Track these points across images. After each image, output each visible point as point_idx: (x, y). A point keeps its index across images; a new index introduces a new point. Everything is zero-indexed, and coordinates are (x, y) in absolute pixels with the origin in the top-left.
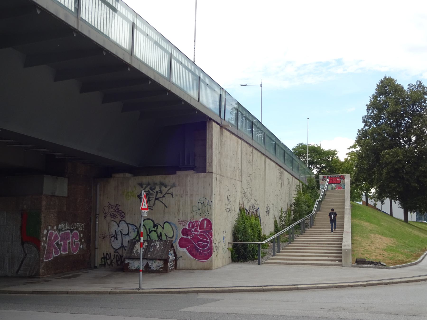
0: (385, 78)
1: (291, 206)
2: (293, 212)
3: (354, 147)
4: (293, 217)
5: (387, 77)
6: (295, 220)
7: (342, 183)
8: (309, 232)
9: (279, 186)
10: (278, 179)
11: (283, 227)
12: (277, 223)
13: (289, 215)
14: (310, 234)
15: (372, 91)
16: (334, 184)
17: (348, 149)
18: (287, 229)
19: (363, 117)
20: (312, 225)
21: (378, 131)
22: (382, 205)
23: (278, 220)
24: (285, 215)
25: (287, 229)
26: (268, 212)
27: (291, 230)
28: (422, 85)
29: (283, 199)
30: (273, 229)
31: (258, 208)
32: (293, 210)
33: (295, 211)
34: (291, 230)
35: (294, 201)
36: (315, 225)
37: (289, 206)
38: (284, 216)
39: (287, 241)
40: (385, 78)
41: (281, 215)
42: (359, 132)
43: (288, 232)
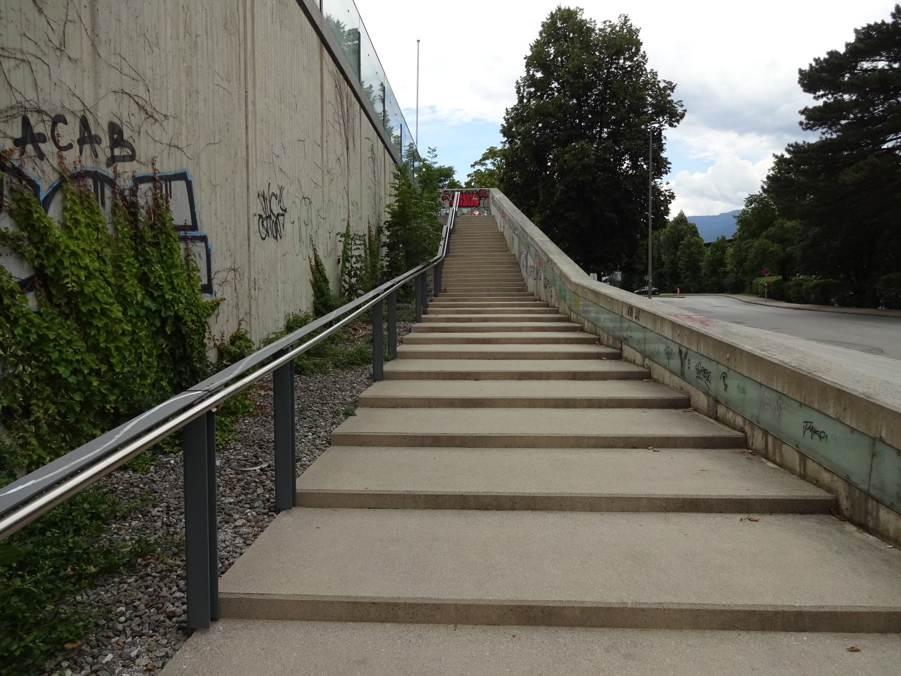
0: (559, 9)
1: (379, 231)
2: (385, 250)
3: (481, 162)
4: (385, 263)
5: (563, 8)
6: (394, 270)
7: (481, 205)
8: (439, 312)
9: (336, 144)
10: (329, 110)
11: (352, 293)
12: (326, 281)
13: (372, 252)
14: (449, 320)
15: (533, 34)
16: (467, 207)
17: (473, 166)
18: (366, 299)
19: (517, 83)
20: (438, 290)
21: (541, 113)
22: (255, 337)
23: (330, 270)
24: (358, 251)
25: (366, 299)
26: (272, 223)
27: (385, 308)
28: (629, 23)
29: (353, 197)
30: (305, 302)
31: (264, 239)
32: (385, 244)
33: (392, 247)
34: (385, 308)
35: (388, 217)
36: (445, 291)
37: (374, 230)
38: (356, 253)
39: (365, 361)
40: (559, 9)
41: (344, 252)
42: (507, 114)
43: (372, 315)
